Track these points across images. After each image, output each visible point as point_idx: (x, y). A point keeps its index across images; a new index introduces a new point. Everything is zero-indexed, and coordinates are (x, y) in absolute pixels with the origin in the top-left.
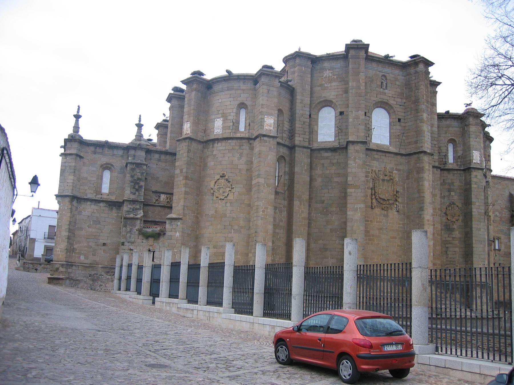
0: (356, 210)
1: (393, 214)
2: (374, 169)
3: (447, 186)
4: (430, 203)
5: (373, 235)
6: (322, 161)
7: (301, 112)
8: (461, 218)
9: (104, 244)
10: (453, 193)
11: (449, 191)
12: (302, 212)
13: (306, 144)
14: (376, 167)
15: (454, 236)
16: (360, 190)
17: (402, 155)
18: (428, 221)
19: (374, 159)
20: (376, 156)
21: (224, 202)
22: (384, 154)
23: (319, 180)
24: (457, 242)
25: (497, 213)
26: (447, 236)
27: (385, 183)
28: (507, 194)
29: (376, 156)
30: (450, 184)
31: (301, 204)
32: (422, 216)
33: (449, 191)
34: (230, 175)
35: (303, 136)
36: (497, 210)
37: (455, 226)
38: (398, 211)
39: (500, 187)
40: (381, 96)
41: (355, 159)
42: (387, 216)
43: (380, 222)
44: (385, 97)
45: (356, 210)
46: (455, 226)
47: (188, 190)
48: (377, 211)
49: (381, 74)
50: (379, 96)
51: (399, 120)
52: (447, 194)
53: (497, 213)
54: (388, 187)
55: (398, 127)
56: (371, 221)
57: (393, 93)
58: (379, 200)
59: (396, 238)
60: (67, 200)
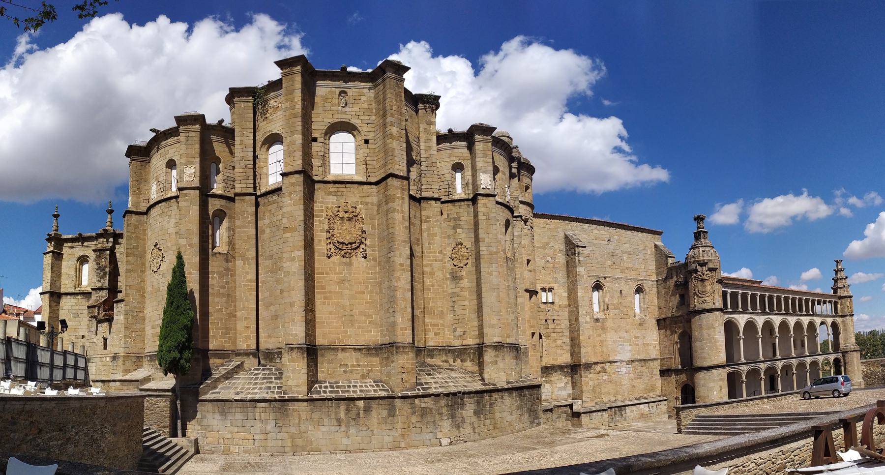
0: (293, 259)
1: (357, 260)
2: (330, 206)
3: (452, 223)
4: (404, 242)
5: (330, 292)
6: (270, 208)
7: (242, 154)
8: (470, 262)
9: (83, 337)
10: (459, 231)
11: (455, 227)
12: (248, 273)
13: (251, 191)
14: (332, 203)
15: (462, 286)
16: (297, 233)
17: (370, 184)
18: (402, 265)
19: (330, 193)
20: (332, 190)
21: (157, 274)
22: (343, 186)
23: (268, 231)
24: (466, 293)
25: (549, 259)
26: (453, 286)
27: (346, 222)
28: (562, 235)
29: (332, 190)
30: (455, 220)
31: (245, 264)
32: (391, 259)
33: (455, 227)
34: (161, 242)
35: (244, 182)
36: (548, 255)
37: (463, 273)
38: (365, 257)
39: (552, 227)
40: (340, 116)
41: (290, 194)
42: (350, 264)
43: (341, 273)
44: (344, 116)
45: (293, 259)
46: (463, 273)
47: (130, 267)
48: (336, 259)
49: (338, 90)
50: (336, 116)
51: (367, 142)
52: (452, 232)
53: (549, 259)
54: (350, 226)
55: (364, 150)
56: (327, 274)
57: (357, 110)
58: (337, 245)
59: (364, 293)
60: (47, 295)
